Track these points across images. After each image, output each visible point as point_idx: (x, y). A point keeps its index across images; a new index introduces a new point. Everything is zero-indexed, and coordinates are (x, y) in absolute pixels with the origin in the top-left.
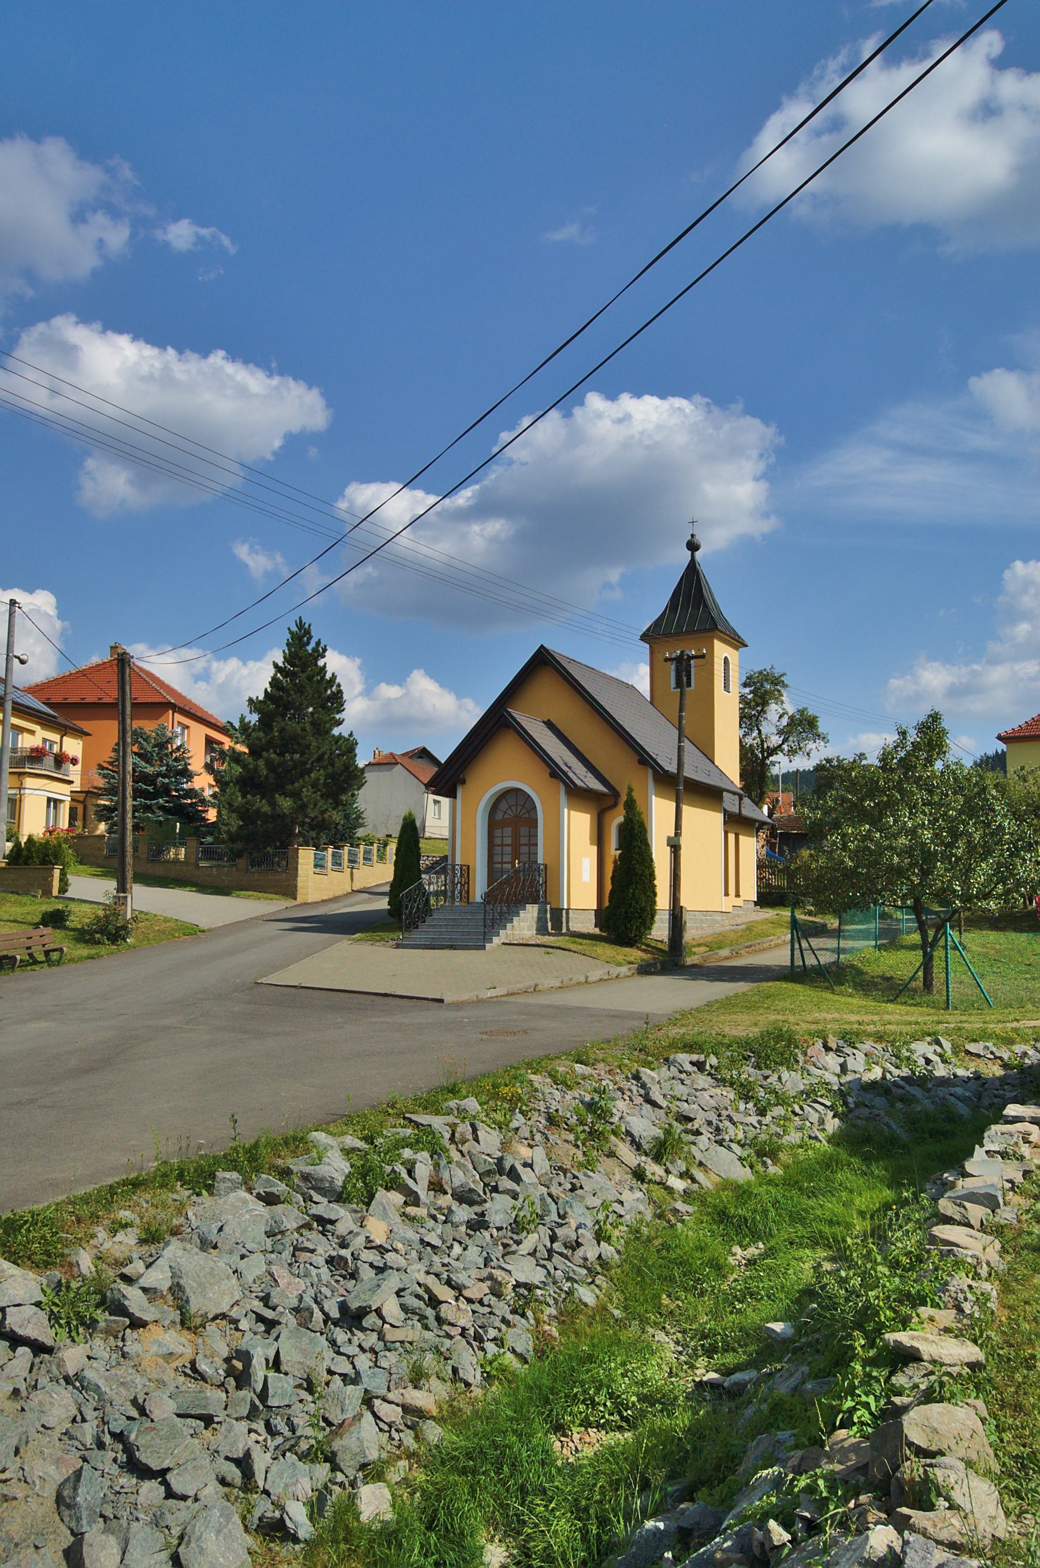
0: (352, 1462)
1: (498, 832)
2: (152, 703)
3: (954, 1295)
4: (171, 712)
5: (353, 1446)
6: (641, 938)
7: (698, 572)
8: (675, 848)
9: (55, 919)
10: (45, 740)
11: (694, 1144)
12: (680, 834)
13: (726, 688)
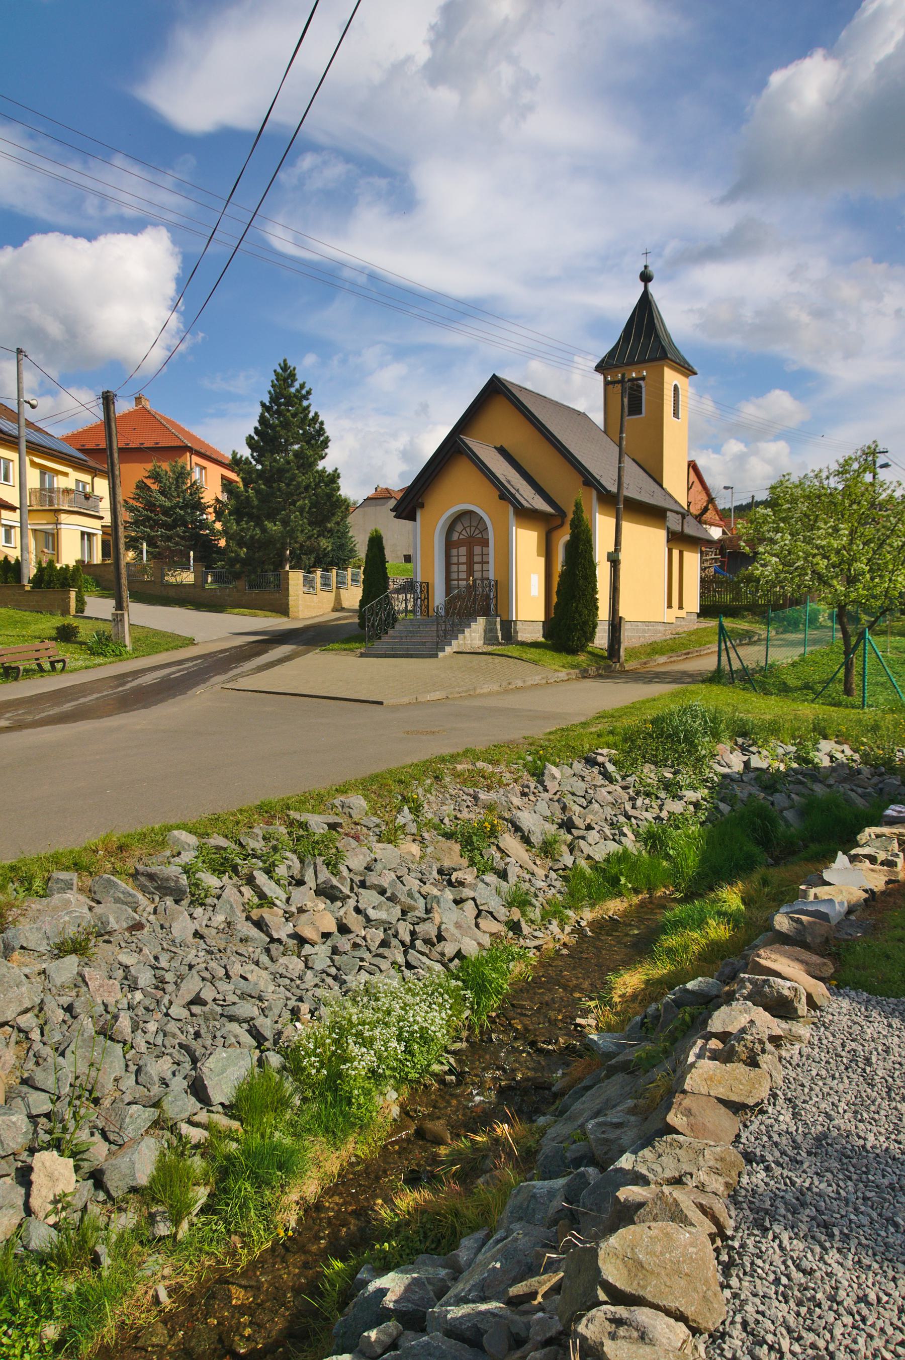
0: (120, 1183)
1: (454, 552)
2: (172, 447)
3: (750, 1045)
4: (188, 454)
5: (123, 1166)
8: (614, 561)
9: (66, 634)
10: (78, 481)
11: (583, 838)
13: (676, 414)
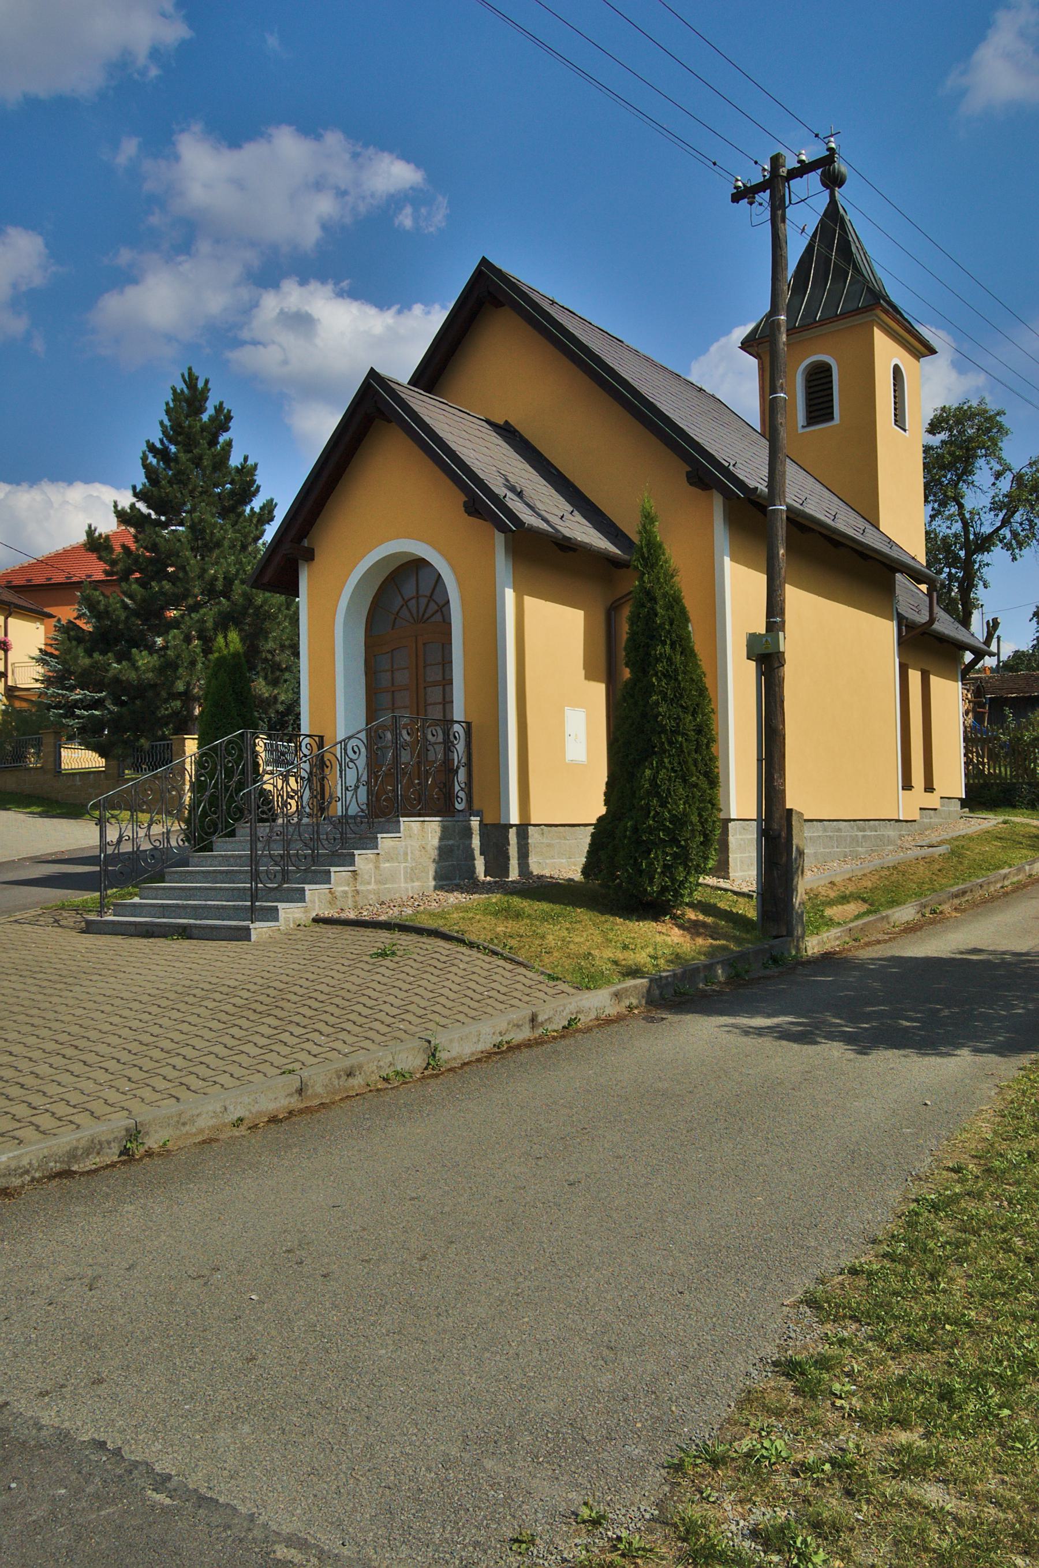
6: (677, 895)
7: (842, 220)
12: (782, 627)
13: (899, 420)
